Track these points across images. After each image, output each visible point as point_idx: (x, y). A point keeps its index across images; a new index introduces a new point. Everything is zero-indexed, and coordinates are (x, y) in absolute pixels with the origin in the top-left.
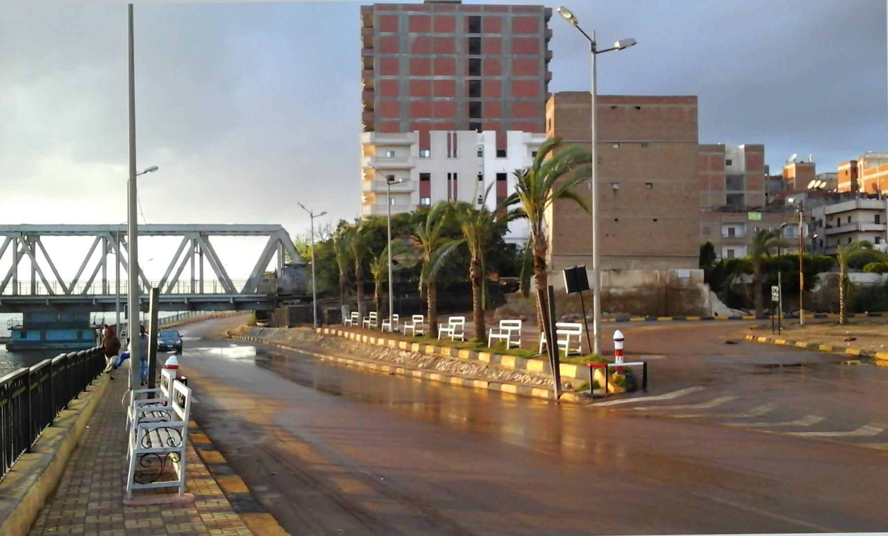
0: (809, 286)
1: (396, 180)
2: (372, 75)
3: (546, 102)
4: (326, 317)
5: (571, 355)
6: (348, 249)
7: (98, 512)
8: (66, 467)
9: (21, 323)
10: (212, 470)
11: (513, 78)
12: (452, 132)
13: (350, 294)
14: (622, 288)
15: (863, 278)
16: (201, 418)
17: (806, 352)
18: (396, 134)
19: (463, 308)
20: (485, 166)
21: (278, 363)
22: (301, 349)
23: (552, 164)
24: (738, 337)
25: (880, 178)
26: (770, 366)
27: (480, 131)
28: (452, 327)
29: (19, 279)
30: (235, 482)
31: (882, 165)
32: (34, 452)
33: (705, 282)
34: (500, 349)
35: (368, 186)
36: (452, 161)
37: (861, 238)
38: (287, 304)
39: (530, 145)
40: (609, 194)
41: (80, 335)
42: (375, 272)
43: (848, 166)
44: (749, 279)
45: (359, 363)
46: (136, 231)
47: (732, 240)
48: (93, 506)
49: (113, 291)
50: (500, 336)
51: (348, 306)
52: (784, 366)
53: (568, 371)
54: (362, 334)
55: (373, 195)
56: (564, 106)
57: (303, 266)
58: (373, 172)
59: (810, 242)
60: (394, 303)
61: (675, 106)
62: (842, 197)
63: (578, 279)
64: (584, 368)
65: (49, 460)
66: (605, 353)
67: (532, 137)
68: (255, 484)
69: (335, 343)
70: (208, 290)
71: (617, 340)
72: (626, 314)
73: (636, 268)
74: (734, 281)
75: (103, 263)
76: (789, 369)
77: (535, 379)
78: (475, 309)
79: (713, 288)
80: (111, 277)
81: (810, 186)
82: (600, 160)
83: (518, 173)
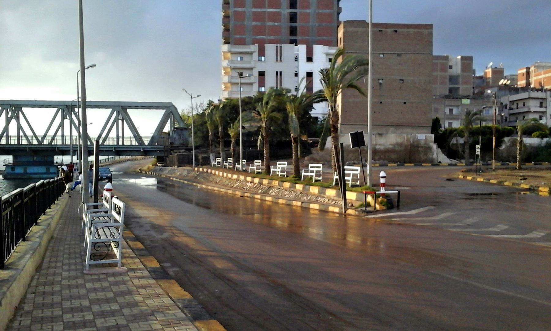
0: (499, 144)
1: (244, 75)
2: (229, 8)
3: (338, 27)
4: (201, 161)
5: (353, 186)
6: (214, 118)
7: (69, 278)
8: (47, 249)
9: (12, 162)
10: (136, 253)
11: (317, 11)
12: (279, 45)
13: (216, 147)
14: (383, 145)
15: (532, 141)
16: (130, 221)
17: (496, 187)
18: (244, 46)
19: (286, 157)
20: (303, 67)
21: (171, 189)
22: (186, 180)
23: (343, 65)
24: (455, 176)
25: (544, 78)
26: (473, 195)
27: (296, 45)
28: (279, 168)
29: (10, 134)
30: (151, 261)
31: (545, 70)
32: (28, 240)
33: (435, 142)
34: (309, 182)
35: (226, 79)
36: (279, 64)
37: (531, 116)
38: (176, 152)
39: (327, 54)
40: (378, 86)
41: (48, 169)
42: (231, 132)
43: (524, 71)
44: (461, 141)
45: (222, 190)
46: (86, 105)
47: (451, 116)
48: (65, 274)
49: (68, 142)
50: (309, 174)
51: (214, 154)
52: (482, 194)
53: (351, 196)
54: (223, 172)
55: (229, 85)
56: (350, 29)
57: (186, 129)
58: (229, 70)
59: (499, 118)
60: (243, 153)
61: (419, 30)
62: (520, 90)
63: (358, 139)
64: (361, 194)
65: (37, 246)
66: (374, 185)
67: (329, 49)
68: (163, 262)
69: (207, 177)
70: (127, 143)
71: (382, 177)
72: (386, 161)
73: (392, 133)
74: (452, 142)
75: (62, 125)
76: (486, 197)
77: (330, 201)
78: (293, 157)
79: (439, 146)
80: (67, 133)
81: (500, 83)
82: (373, 64)
83: (322, 71)
